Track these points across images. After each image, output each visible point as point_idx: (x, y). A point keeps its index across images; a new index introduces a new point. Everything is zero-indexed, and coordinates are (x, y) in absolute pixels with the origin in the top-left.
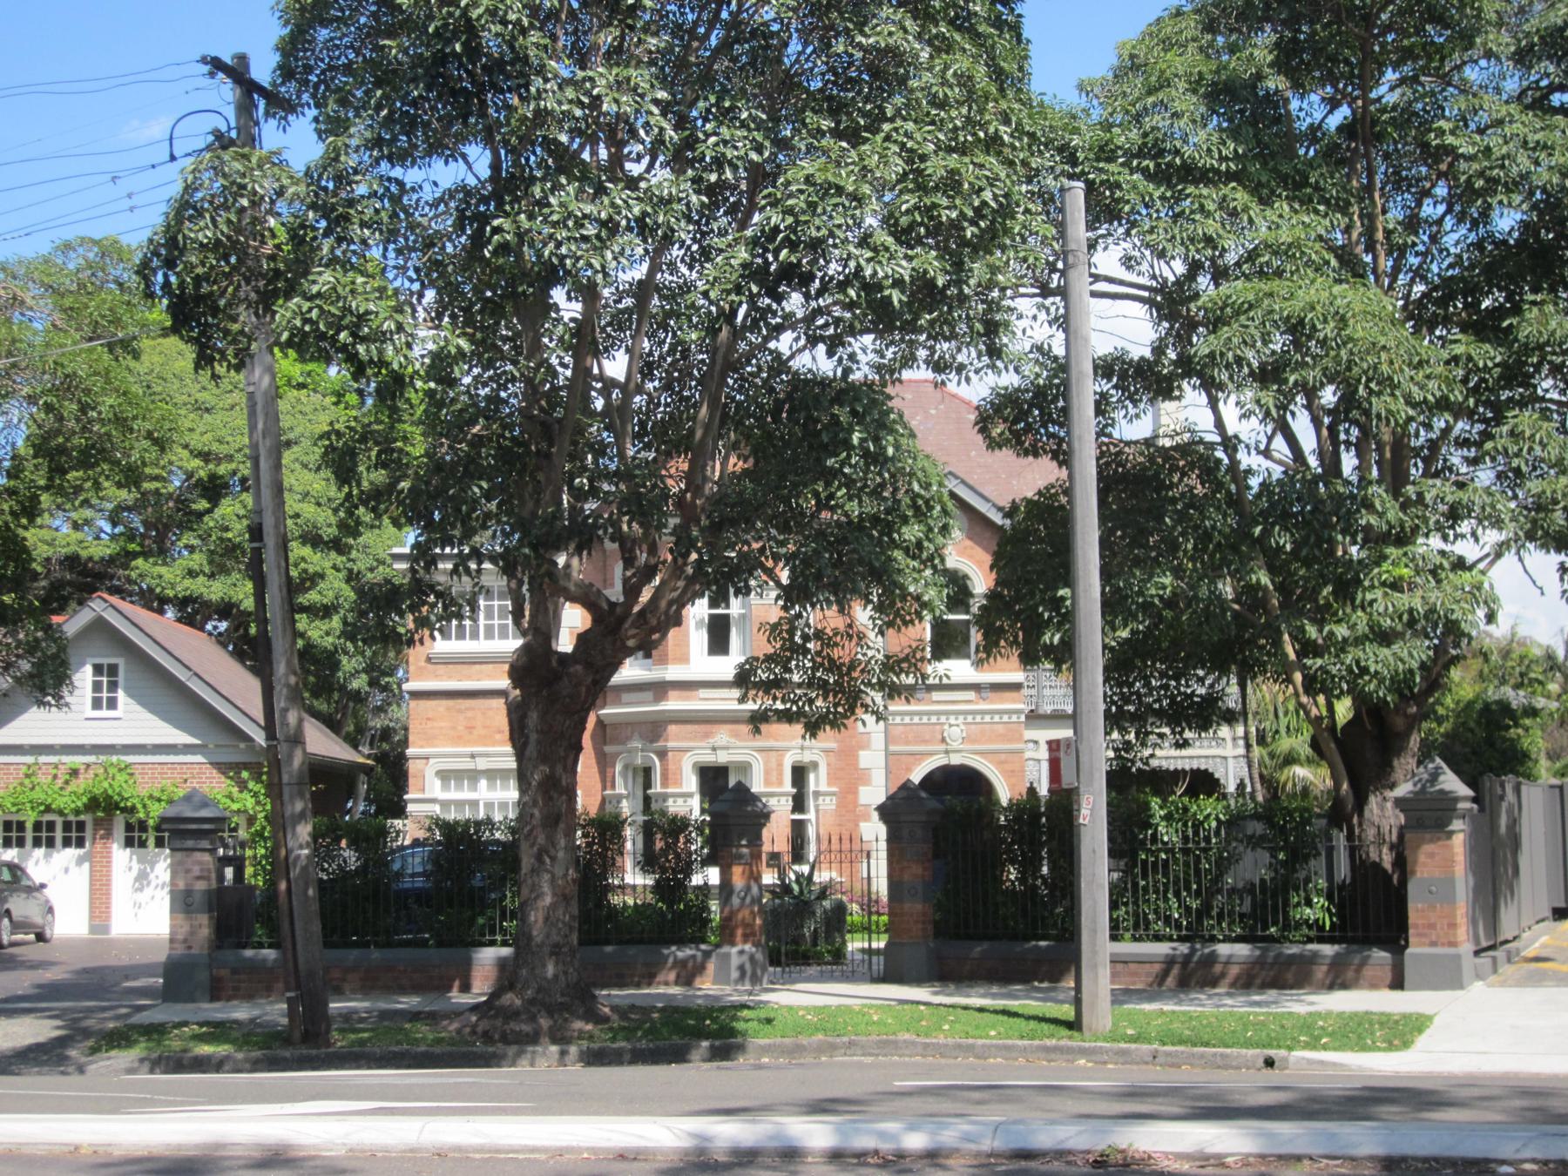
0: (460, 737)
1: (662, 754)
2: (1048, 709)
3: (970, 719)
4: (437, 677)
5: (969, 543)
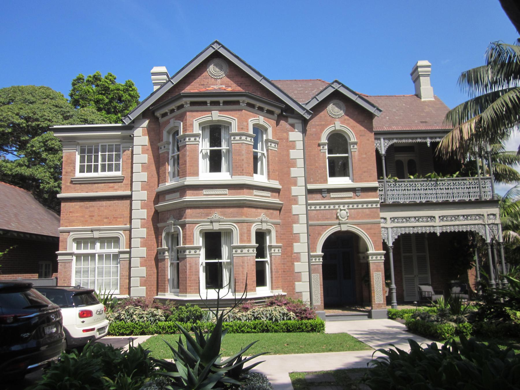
0: (86, 221)
1: (183, 226)
2: (390, 201)
3: (351, 206)
4: (76, 191)
5: (347, 117)
